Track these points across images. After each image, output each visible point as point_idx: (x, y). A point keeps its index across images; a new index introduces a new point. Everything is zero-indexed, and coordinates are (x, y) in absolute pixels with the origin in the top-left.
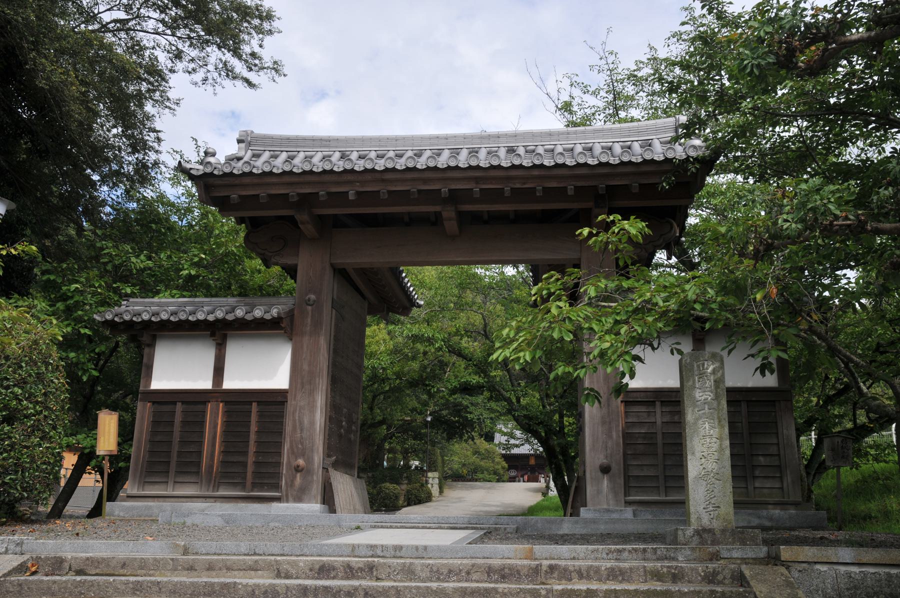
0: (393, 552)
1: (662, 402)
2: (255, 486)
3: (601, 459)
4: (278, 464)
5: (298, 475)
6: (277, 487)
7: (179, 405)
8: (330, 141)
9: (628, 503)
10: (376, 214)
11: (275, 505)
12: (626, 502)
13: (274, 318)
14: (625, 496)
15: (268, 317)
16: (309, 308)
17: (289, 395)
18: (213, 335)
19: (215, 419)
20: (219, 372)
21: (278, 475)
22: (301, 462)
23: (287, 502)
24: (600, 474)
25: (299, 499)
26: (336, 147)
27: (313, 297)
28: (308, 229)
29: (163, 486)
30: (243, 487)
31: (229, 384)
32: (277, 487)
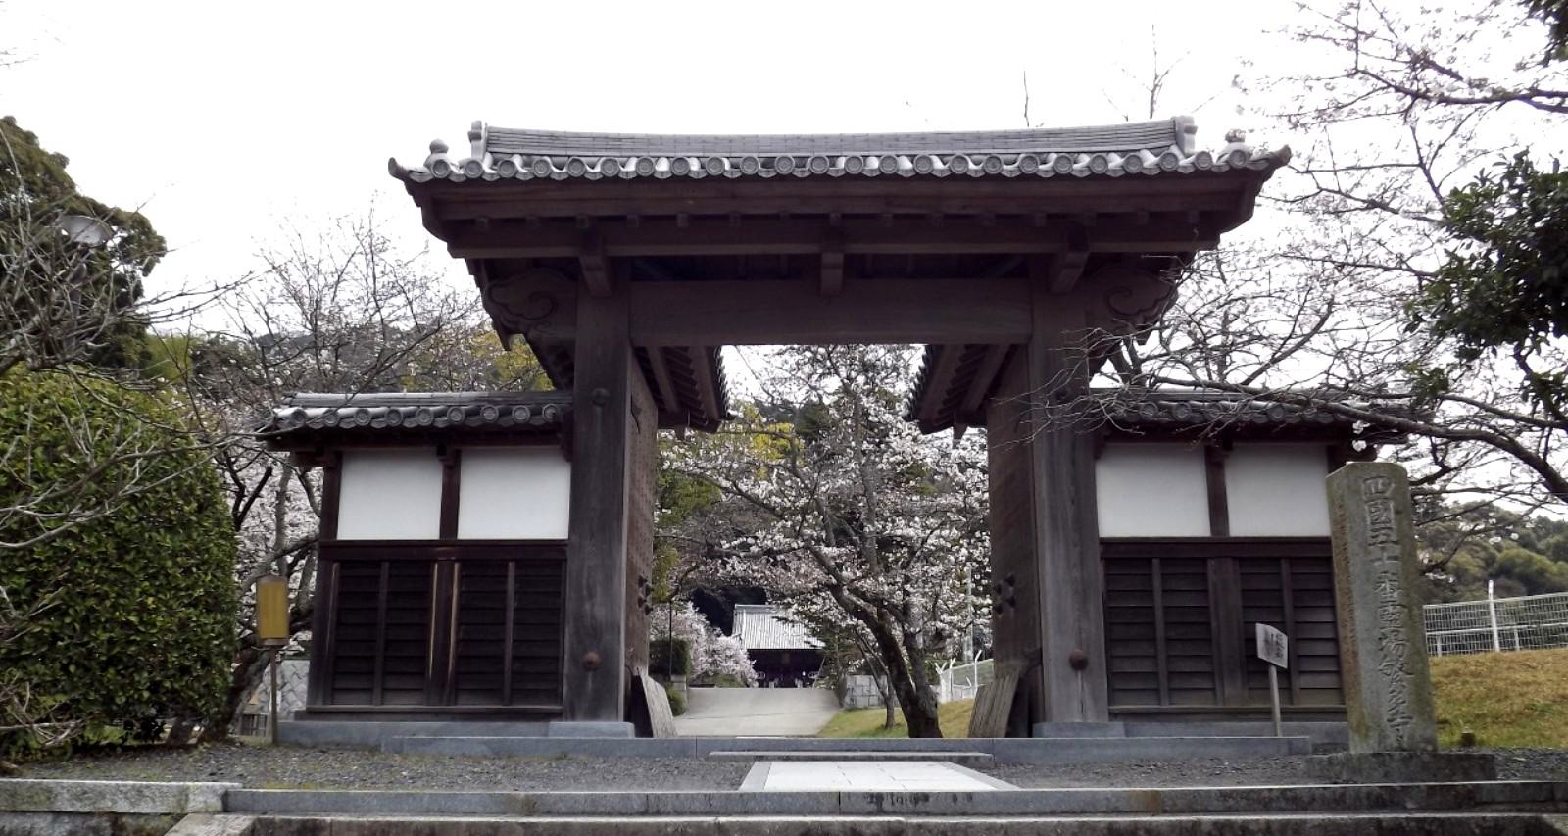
0: (911, 805)
1: (1162, 559)
2: (518, 693)
3: (1072, 648)
4: (557, 659)
5: (590, 675)
6: (555, 695)
7: (1285, 565)
8: (620, 140)
9: (1114, 715)
10: (692, 258)
11: (555, 724)
12: (1110, 714)
13: (547, 424)
14: (1109, 704)
15: (537, 421)
16: (598, 409)
17: (567, 549)
18: (441, 452)
19: (448, 589)
20: (1218, 508)
21: (556, 677)
22: (593, 656)
23: (573, 718)
24: (1069, 670)
25: (593, 714)
26: (632, 149)
27: (604, 391)
28: (596, 278)
29: (364, 696)
30: (494, 692)
31: (469, 529)
32: (555, 695)
